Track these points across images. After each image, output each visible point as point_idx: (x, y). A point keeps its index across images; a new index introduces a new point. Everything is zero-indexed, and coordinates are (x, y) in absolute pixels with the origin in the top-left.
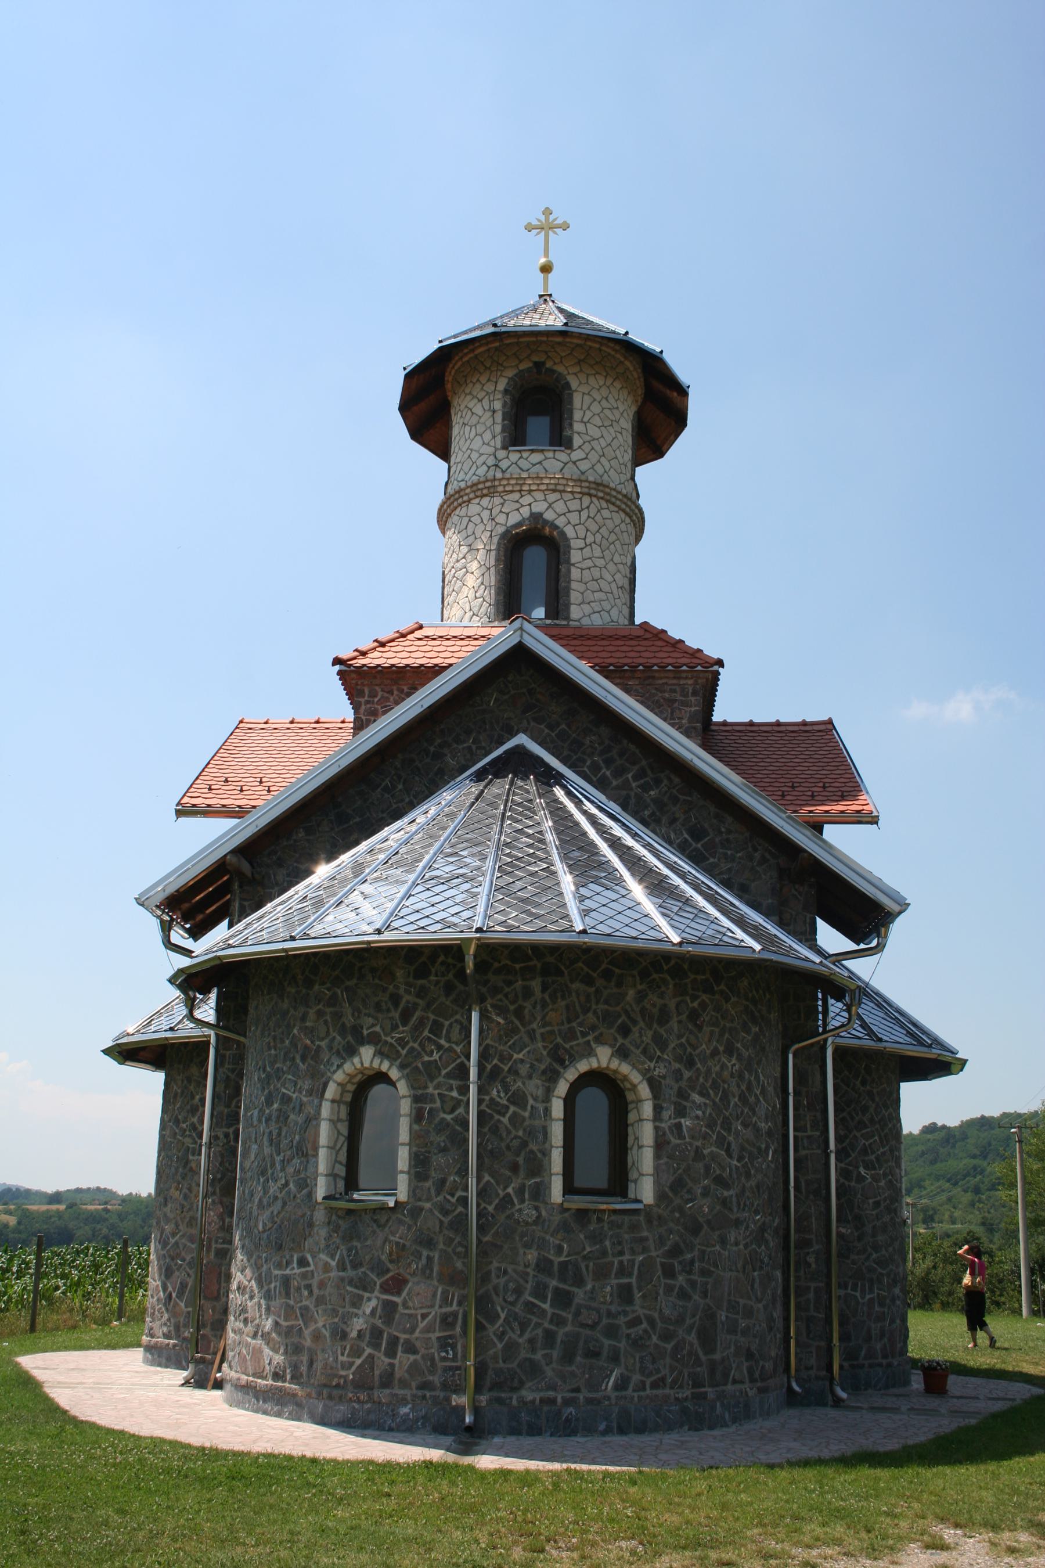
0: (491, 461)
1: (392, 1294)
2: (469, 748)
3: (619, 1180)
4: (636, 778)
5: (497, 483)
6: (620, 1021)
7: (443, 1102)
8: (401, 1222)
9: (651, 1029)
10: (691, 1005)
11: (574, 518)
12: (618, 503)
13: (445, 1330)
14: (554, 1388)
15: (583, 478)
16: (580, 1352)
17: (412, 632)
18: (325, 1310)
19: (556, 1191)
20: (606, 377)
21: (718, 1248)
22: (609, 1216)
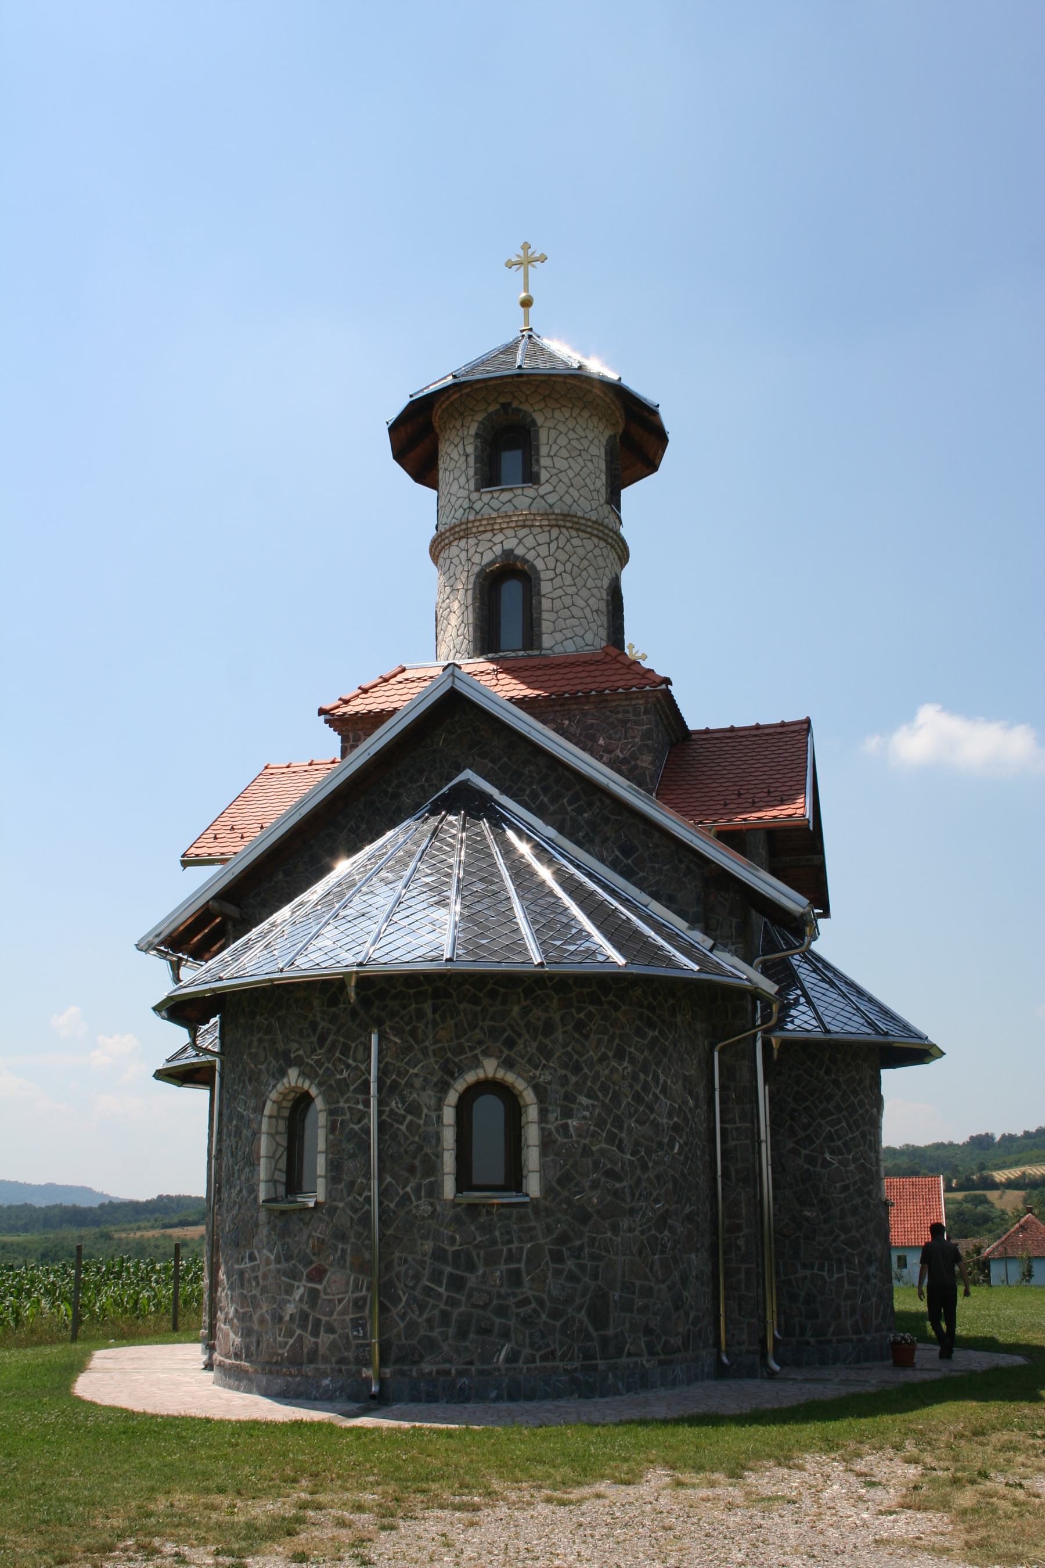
0: (466, 505)
1: (315, 1282)
2: (422, 786)
3: (515, 1179)
4: (570, 803)
5: (470, 525)
6: (505, 1035)
7: (352, 1114)
8: (321, 1220)
9: (535, 1040)
10: (577, 1016)
11: (543, 550)
12: (589, 530)
13: (356, 1313)
14: (449, 1361)
15: (550, 511)
16: (473, 1329)
17: (395, 676)
18: (267, 1298)
19: (449, 1188)
20: (572, 409)
21: (609, 1234)
22: (498, 1209)
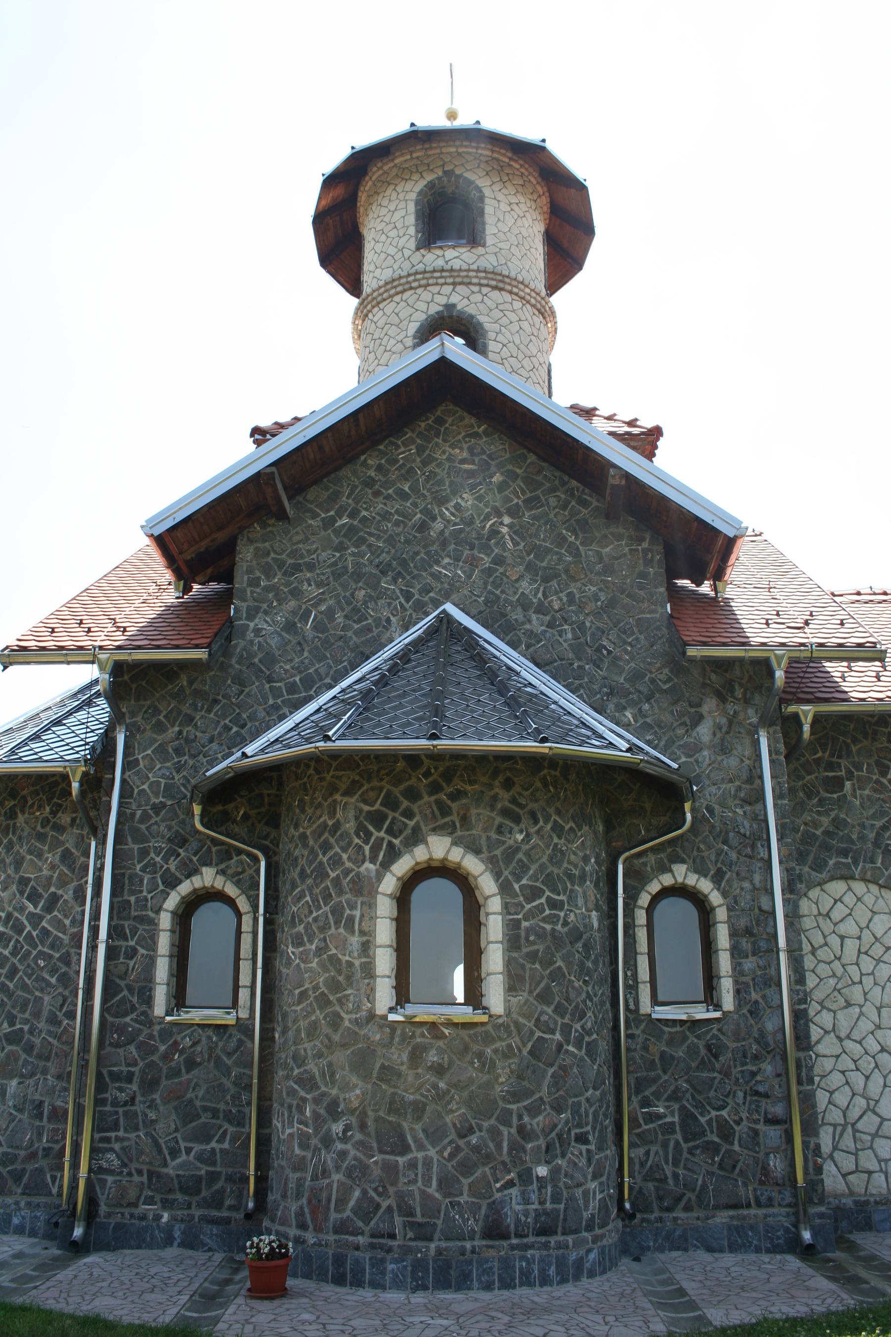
12: (385, 295)
